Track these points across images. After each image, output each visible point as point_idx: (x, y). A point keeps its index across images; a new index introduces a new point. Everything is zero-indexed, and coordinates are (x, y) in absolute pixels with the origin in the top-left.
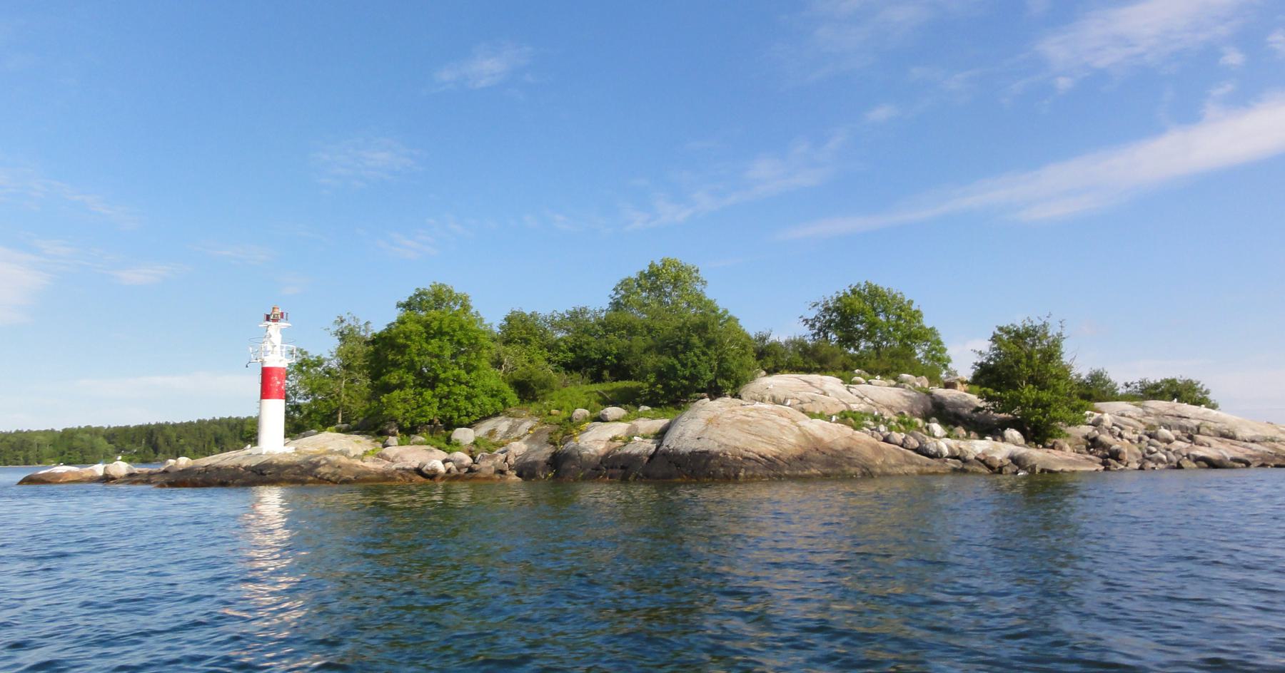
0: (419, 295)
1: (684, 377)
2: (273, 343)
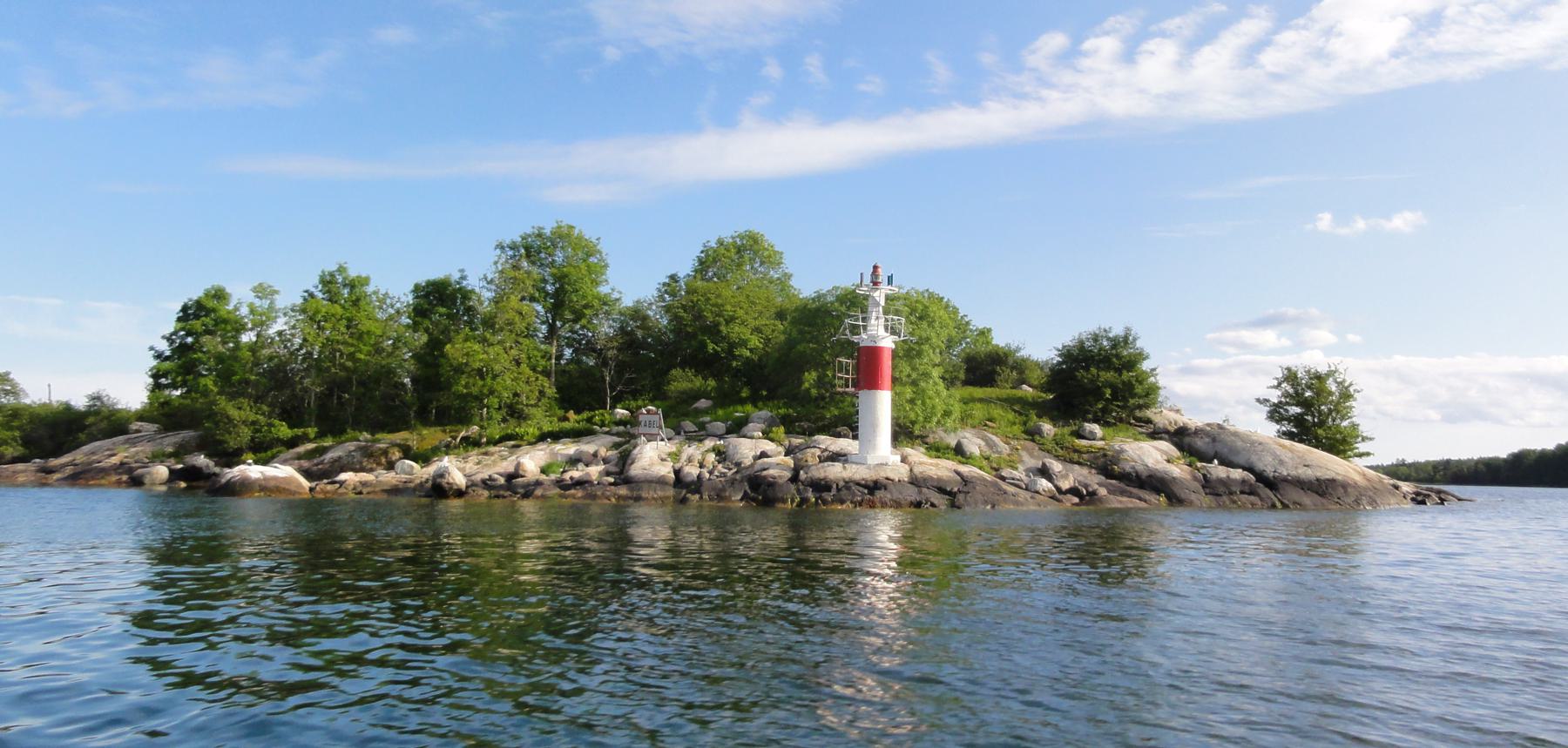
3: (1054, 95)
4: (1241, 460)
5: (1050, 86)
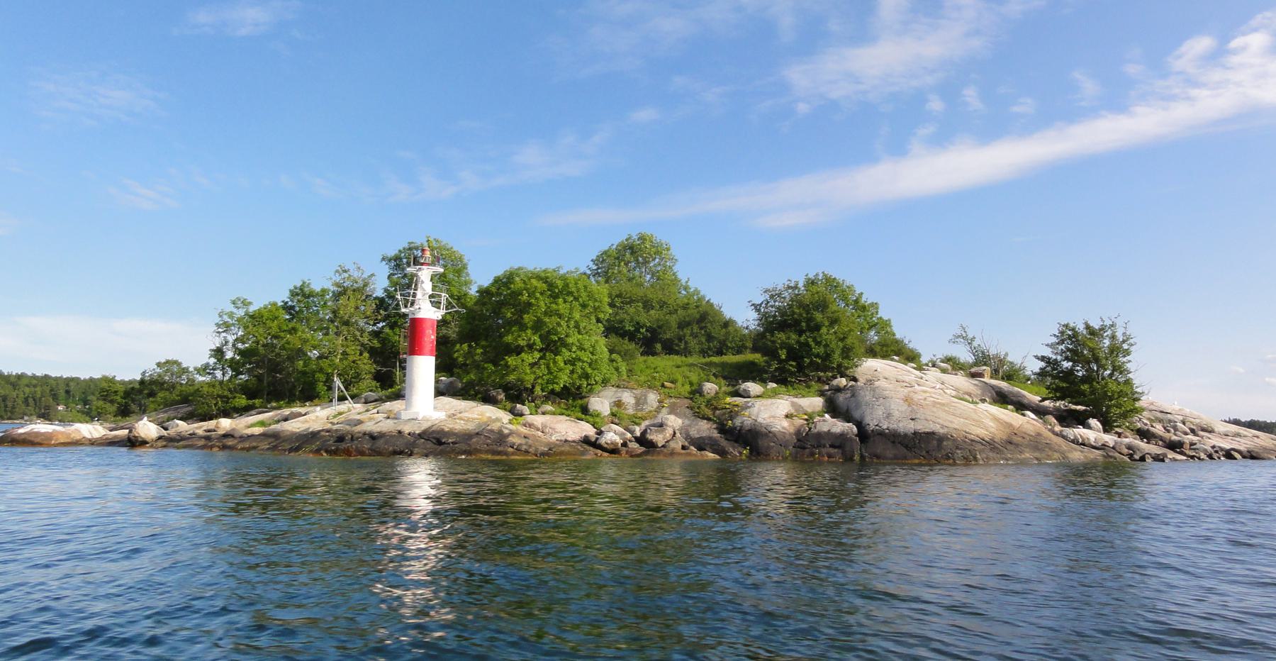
0: (410, 249)
1: (818, 356)
2: (425, 290)
3: (1205, 92)
4: (857, 415)
5: (1196, 84)
